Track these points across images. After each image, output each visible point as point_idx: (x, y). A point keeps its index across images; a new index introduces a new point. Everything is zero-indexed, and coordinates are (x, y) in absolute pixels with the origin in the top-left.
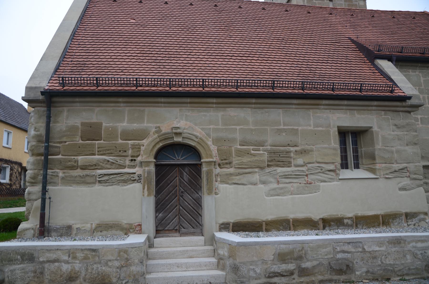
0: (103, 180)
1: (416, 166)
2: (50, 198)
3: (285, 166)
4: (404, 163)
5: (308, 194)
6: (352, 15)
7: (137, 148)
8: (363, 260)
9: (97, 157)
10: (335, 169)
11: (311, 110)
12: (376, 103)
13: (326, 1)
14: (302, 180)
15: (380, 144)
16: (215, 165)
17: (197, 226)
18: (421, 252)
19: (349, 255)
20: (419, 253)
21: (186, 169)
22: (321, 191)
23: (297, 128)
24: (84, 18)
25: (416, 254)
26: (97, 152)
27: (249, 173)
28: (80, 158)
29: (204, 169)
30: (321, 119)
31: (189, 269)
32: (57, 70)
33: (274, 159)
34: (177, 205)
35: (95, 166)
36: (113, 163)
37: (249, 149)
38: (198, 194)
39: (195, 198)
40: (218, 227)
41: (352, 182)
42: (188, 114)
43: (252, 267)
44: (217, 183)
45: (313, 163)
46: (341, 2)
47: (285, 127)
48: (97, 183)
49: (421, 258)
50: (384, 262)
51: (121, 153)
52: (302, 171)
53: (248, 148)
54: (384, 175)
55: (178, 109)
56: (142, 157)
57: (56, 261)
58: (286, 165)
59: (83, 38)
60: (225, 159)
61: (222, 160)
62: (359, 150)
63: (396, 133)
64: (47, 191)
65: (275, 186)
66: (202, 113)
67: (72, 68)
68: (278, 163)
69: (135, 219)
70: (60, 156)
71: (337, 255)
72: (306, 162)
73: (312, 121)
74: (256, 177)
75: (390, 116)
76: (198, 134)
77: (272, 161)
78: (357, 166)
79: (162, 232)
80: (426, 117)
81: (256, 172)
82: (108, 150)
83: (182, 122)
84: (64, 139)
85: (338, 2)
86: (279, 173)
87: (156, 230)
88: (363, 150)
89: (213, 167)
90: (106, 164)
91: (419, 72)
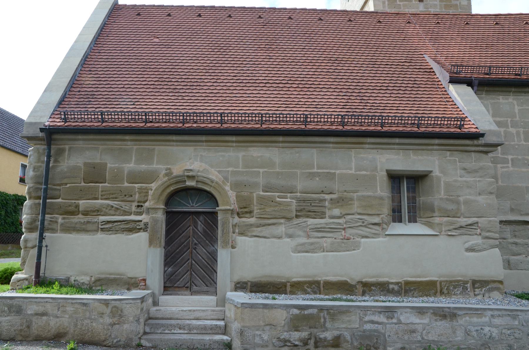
0: (109, 228)
1: (490, 221)
2: (46, 246)
3: (318, 217)
4: (474, 217)
5: (344, 251)
6: (438, 23)
7: (145, 192)
8: (397, 333)
9: (100, 201)
10: (381, 222)
11: (353, 150)
12: (437, 141)
13: (414, 2)
14: (337, 235)
15: (442, 193)
16: (232, 214)
17: (211, 284)
18: (476, 328)
19: (380, 327)
20: (473, 329)
21: (201, 218)
22: (361, 249)
23: (333, 171)
24: (100, 37)
25: (470, 331)
26: (100, 196)
27: (274, 224)
28: (81, 202)
29: (220, 217)
30: (365, 162)
31: (192, 332)
32: (61, 103)
33: (304, 209)
34: (189, 259)
35: (98, 212)
36: (117, 209)
37: (274, 196)
38: (214, 246)
39: (210, 251)
40: (233, 286)
41: (402, 240)
42: (203, 154)
43: (258, 333)
44: (234, 235)
45: (353, 214)
46: (435, 3)
47: (319, 171)
48: (99, 231)
49: (476, 336)
50: (426, 338)
51: (125, 198)
52: (339, 223)
53: (272, 195)
54: (445, 231)
55: (192, 148)
56: (150, 202)
57: (43, 314)
58: (319, 215)
59: (96, 63)
60: (245, 208)
61: (241, 208)
62: (417, 199)
63: (464, 179)
64: (44, 239)
65: (304, 240)
66: (220, 154)
67: (79, 100)
68: (309, 213)
69: (138, 273)
70: (60, 200)
71: (365, 325)
72: (344, 213)
73: (353, 164)
74: (281, 229)
75: (457, 157)
76: (214, 178)
77: (301, 210)
78: (413, 219)
79: (170, 289)
80: (520, 157)
81: (281, 223)
82: (113, 194)
83: (196, 163)
84: (65, 181)
85: (431, 3)
86: (310, 225)
87: (164, 287)
88: (422, 199)
89: (229, 215)
90: (110, 210)
91: (513, 99)
